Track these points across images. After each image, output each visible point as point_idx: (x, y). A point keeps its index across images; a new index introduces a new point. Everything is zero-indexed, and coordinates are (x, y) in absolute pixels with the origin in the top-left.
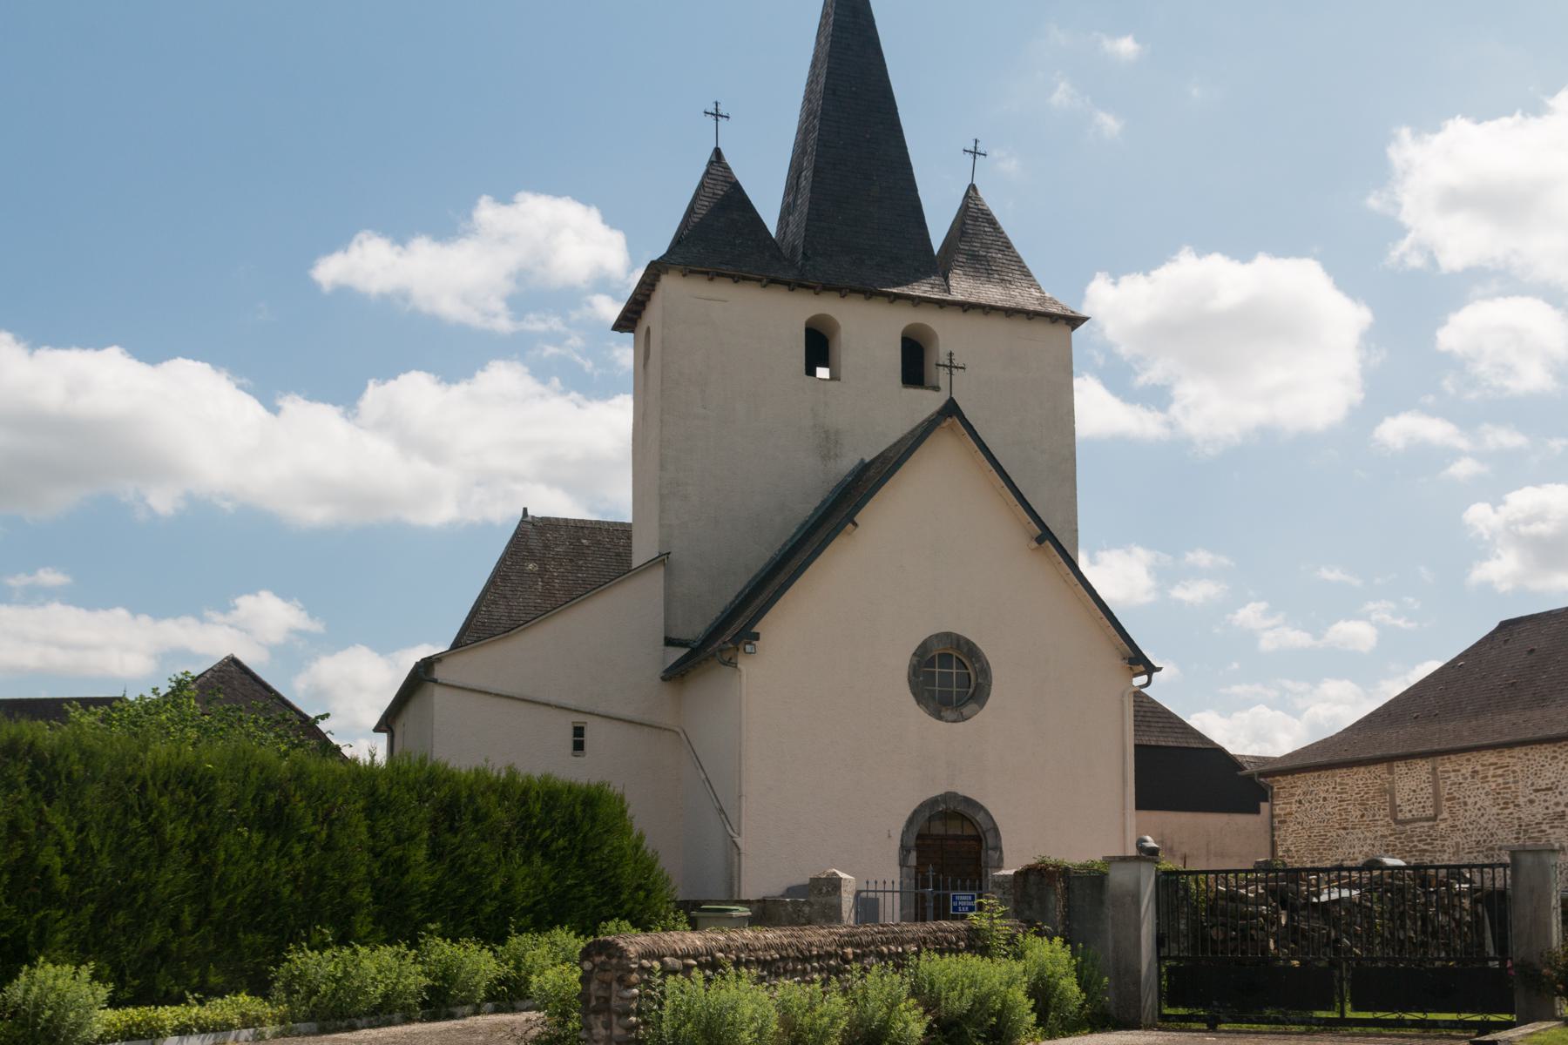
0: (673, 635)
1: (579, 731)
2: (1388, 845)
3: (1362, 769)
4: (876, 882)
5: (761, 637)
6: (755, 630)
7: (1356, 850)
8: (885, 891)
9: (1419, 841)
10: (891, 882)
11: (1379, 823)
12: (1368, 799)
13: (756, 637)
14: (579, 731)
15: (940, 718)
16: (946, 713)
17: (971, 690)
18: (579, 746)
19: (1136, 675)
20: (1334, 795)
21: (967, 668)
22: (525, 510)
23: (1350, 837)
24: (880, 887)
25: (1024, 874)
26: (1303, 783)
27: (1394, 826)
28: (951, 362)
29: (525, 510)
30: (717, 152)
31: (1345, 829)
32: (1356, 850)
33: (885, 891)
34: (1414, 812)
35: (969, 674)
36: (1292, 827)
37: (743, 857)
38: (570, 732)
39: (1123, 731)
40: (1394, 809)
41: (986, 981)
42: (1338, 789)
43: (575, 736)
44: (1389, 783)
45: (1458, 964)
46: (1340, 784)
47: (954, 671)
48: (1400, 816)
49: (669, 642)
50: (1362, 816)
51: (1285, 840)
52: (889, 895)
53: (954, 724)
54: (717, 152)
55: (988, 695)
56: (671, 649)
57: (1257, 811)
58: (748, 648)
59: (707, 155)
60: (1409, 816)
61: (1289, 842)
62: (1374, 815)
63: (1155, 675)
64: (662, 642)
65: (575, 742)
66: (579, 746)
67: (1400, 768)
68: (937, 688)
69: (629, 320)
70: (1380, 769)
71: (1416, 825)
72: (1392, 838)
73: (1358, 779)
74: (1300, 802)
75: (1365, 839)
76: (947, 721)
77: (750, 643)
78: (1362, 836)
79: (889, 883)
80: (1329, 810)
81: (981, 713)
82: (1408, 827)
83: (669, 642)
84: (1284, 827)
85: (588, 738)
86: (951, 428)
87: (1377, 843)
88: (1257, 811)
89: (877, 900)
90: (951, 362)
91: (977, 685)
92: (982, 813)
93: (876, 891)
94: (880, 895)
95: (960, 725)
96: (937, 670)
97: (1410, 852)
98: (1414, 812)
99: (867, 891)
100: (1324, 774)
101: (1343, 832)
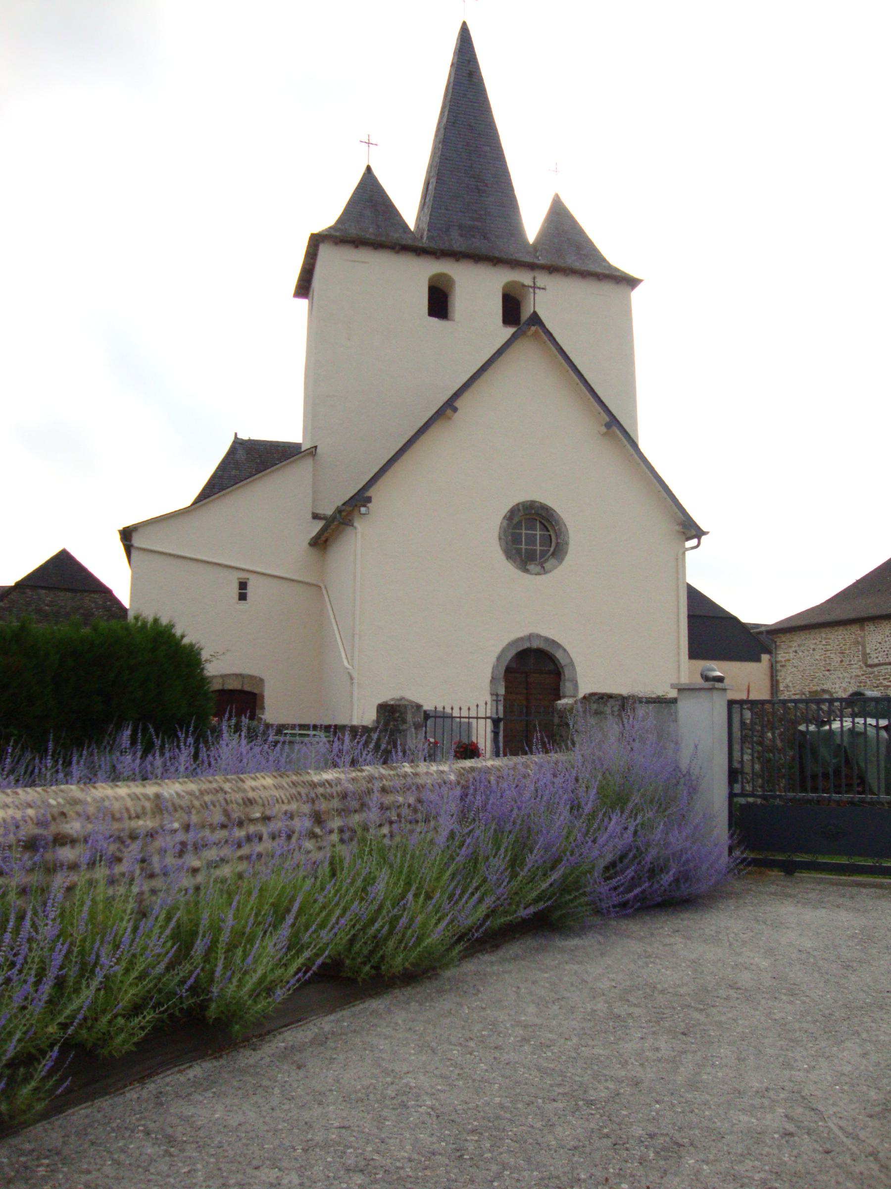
0: (317, 511)
1: (243, 585)
2: (860, 682)
3: (841, 628)
4: (460, 709)
5: (373, 500)
6: (368, 494)
7: (837, 686)
8: (477, 718)
9: (884, 679)
10: (466, 708)
11: (854, 666)
12: (845, 649)
13: (369, 500)
14: (243, 585)
15: (526, 571)
16: (532, 567)
17: (552, 549)
18: (243, 597)
19: (688, 539)
20: (820, 646)
21: (548, 531)
22: (236, 434)
23: (833, 677)
24: (473, 714)
25: (584, 698)
26: (797, 640)
27: (865, 668)
28: (534, 283)
29: (236, 434)
30: (369, 169)
31: (828, 670)
32: (837, 686)
33: (477, 718)
34: (880, 658)
35: (550, 536)
36: (790, 669)
37: (355, 686)
38: (236, 586)
39: (678, 596)
40: (865, 655)
41: (351, 1162)
42: (824, 642)
43: (240, 589)
44: (862, 637)
45: (770, 740)
46: (825, 639)
47: (538, 533)
48: (870, 662)
49: (316, 516)
50: (842, 661)
51: (785, 679)
52: (481, 722)
53: (538, 577)
54: (369, 169)
55: (566, 553)
56: (316, 521)
57: (758, 660)
58: (363, 510)
59: (362, 171)
60: (876, 661)
61: (788, 680)
62: (850, 661)
63: (703, 538)
64: (310, 516)
65: (240, 593)
66: (243, 597)
67: (870, 627)
68: (523, 546)
69: (304, 288)
70: (855, 628)
71: (882, 667)
72: (863, 677)
73: (838, 638)
74: (796, 652)
75: (844, 679)
76: (532, 574)
77: (364, 506)
78: (841, 676)
79: (473, 708)
80: (818, 657)
81: (561, 567)
82: (875, 669)
83: (316, 516)
84: (784, 669)
85: (250, 591)
86: (536, 335)
87: (853, 681)
88: (758, 660)
89: (469, 724)
90: (534, 283)
91: (557, 544)
92: (561, 651)
93: (469, 718)
94: (474, 721)
95: (543, 577)
96: (524, 532)
97: (877, 687)
98: (880, 658)
99: (460, 717)
100: (813, 632)
101: (827, 673)
